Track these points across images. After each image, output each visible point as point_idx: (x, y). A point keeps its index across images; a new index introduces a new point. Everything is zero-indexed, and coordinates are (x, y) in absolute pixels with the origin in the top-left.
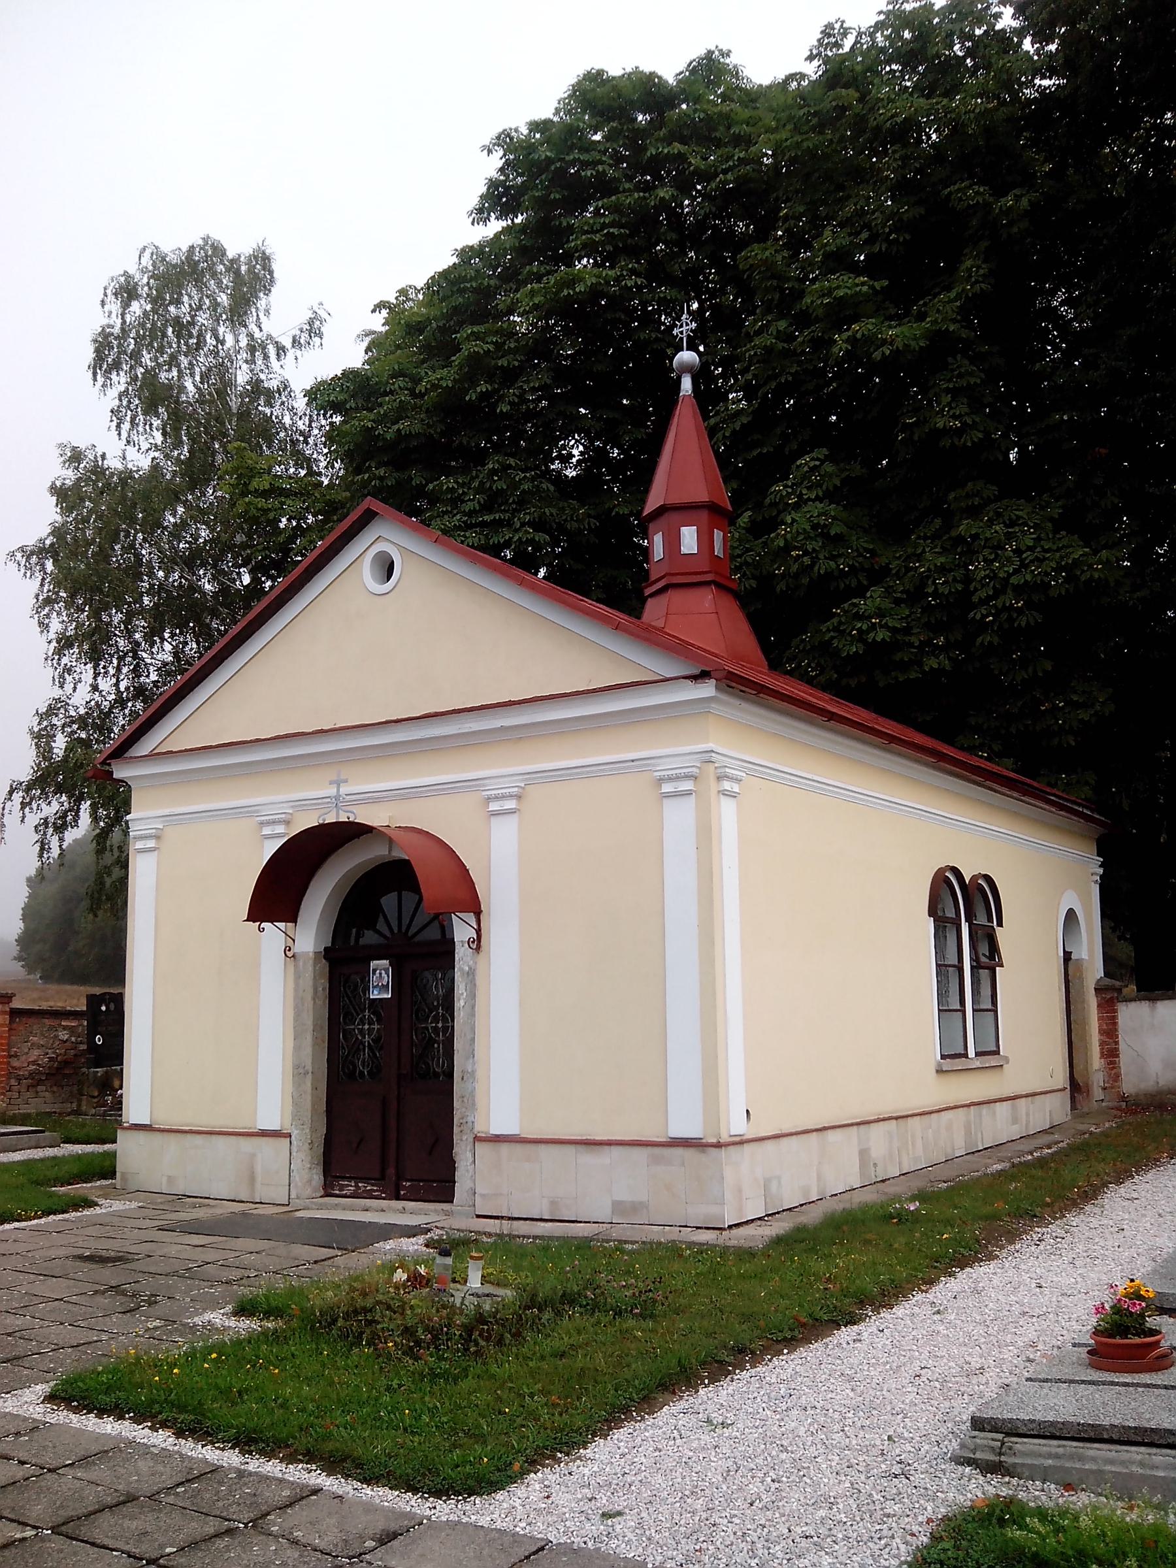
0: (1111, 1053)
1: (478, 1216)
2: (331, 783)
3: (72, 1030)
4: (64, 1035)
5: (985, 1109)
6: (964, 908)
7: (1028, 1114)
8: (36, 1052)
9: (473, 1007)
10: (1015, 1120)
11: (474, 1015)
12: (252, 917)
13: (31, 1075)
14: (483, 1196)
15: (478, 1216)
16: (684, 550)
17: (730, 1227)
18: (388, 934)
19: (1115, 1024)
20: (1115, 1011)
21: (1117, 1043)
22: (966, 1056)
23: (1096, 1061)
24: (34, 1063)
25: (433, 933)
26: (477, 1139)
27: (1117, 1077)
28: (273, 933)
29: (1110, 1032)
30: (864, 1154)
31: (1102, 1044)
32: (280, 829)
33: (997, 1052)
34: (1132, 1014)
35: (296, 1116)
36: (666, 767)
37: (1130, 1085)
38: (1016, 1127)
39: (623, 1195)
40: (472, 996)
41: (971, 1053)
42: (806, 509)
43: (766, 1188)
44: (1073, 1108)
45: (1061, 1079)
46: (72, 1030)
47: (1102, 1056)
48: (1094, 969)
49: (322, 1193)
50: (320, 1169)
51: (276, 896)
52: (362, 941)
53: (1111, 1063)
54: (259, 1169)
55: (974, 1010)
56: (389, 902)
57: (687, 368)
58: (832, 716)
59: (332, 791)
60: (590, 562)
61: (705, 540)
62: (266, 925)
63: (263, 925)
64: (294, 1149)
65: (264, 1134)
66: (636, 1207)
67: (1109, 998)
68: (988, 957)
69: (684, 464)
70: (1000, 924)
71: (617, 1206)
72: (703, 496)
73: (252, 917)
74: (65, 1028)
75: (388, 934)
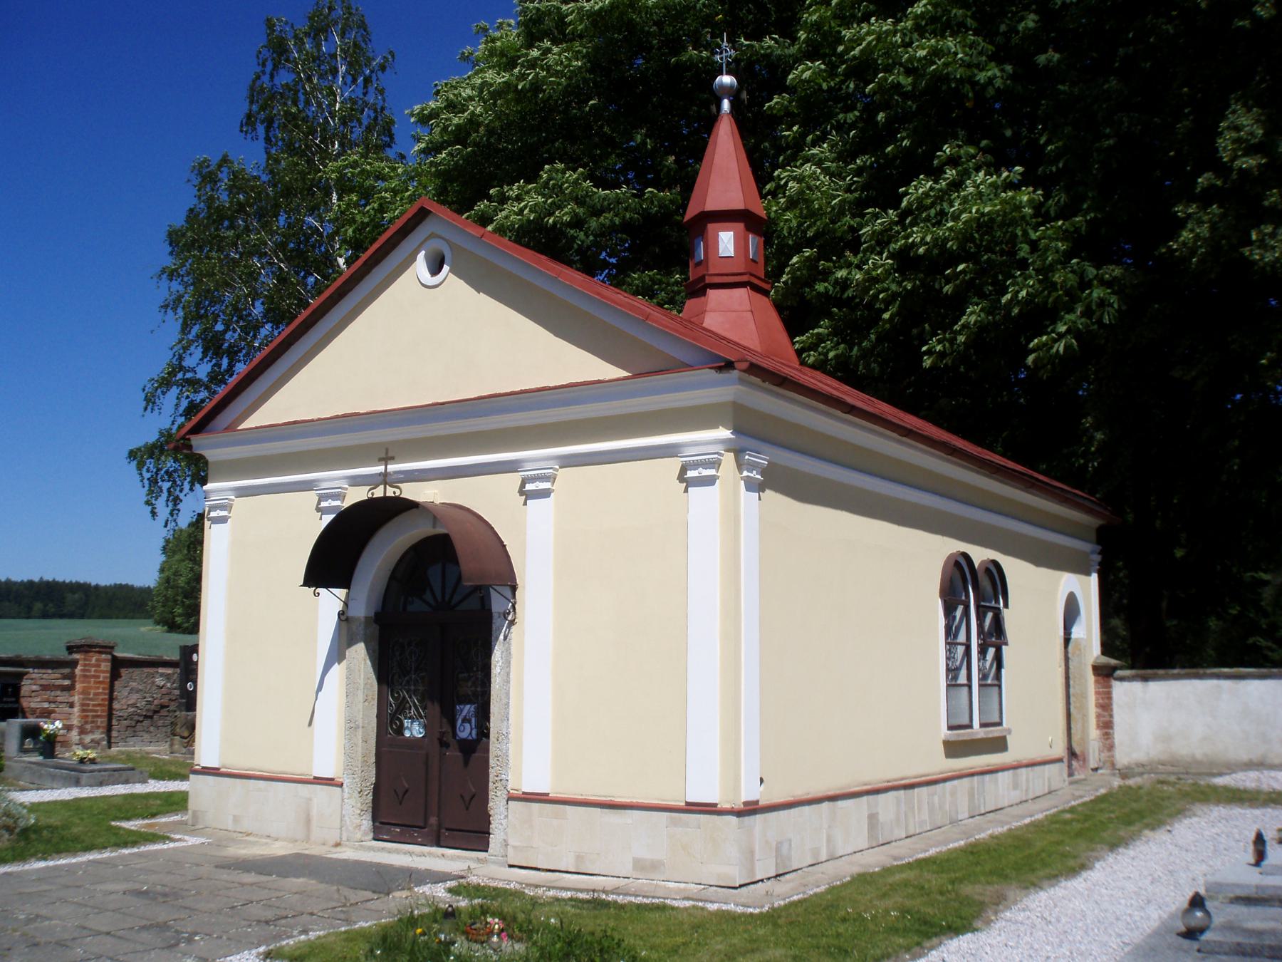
0: (1106, 726)
1: (511, 866)
2: (380, 460)
3: (168, 677)
4: (160, 681)
5: (987, 777)
6: (972, 594)
7: (1028, 781)
8: (134, 697)
9: (508, 674)
10: (1016, 786)
11: (508, 682)
12: (307, 583)
13: (130, 716)
14: (514, 847)
15: (511, 866)
16: (722, 253)
17: (741, 886)
18: (439, 599)
19: (1110, 698)
20: (1110, 687)
21: (1111, 716)
22: (970, 726)
23: (1094, 733)
24: (133, 705)
25: (473, 604)
26: (511, 798)
27: (1111, 747)
28: (330, 601)
29: (1105, 705)
30: (872, 818)
31: (1098, 716)
32: (337, 503)
33: (1000, 724)
34: (1126, 692)
35: (348, 766)
36: (691, 454)
37: (1123, 756)
38: (1018, 792)
39: (646, 854)
40: (508, 663)
41: (976, 724)
42: (816, 175)
43: (778, 849)
44: (1071, 774)
45: (1060, 750)
46: (168, 677)
47: (1098, 727)
48: (1093, 650)
49: (371, 835)
50: (369, 816)
51: (330, 562)
52: (410, 608)
53: (1107, 734)
54: (314, 812)
55: (980, 686)
56: (434, 573)
57: (727, 91)
58: (851, 410)
59: (381, 469)
60: (629, 258)
61: (740, 244)
62: (321, 590)
63: (319, 590)
64: (346, 795)
65: (319, 781)
66: (655, 866)
67: (1104, 673)
68: (995, 635)
69: (725, 176)
70: (1006, 606)
71: (639, 864)
72: (739, 205)
73: (307, 583)
74: (162, 675)
75: (439, 599)
